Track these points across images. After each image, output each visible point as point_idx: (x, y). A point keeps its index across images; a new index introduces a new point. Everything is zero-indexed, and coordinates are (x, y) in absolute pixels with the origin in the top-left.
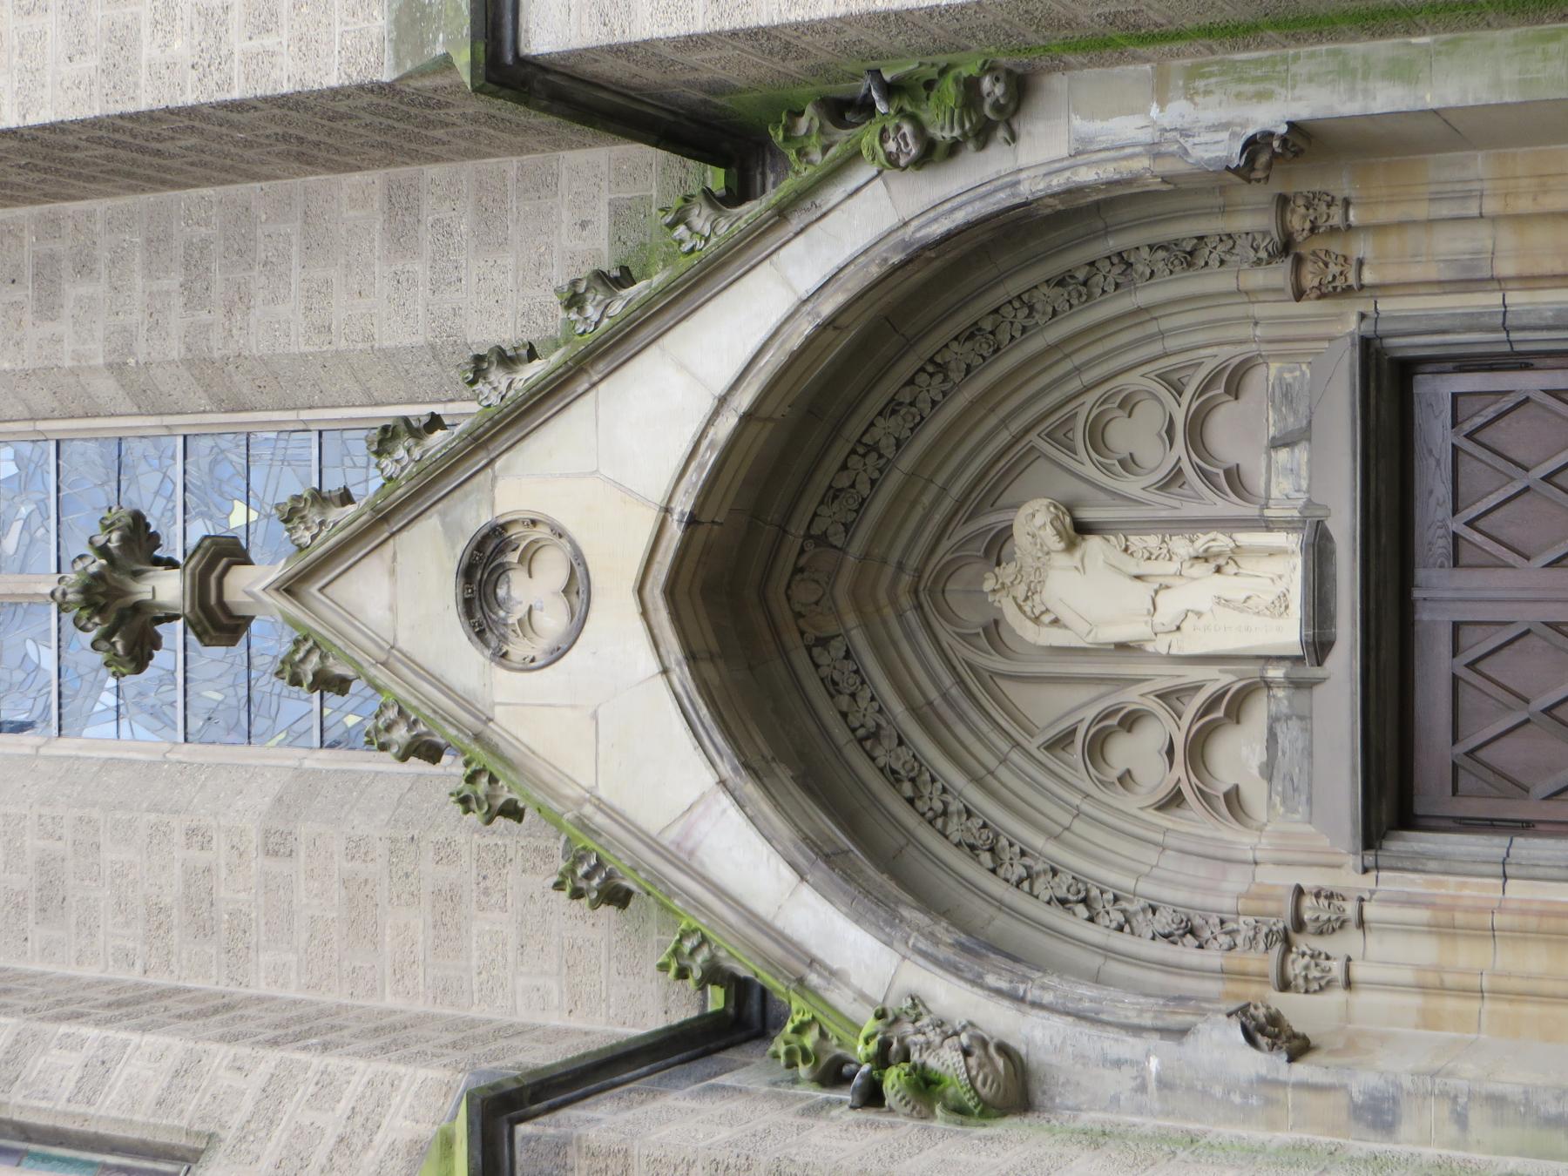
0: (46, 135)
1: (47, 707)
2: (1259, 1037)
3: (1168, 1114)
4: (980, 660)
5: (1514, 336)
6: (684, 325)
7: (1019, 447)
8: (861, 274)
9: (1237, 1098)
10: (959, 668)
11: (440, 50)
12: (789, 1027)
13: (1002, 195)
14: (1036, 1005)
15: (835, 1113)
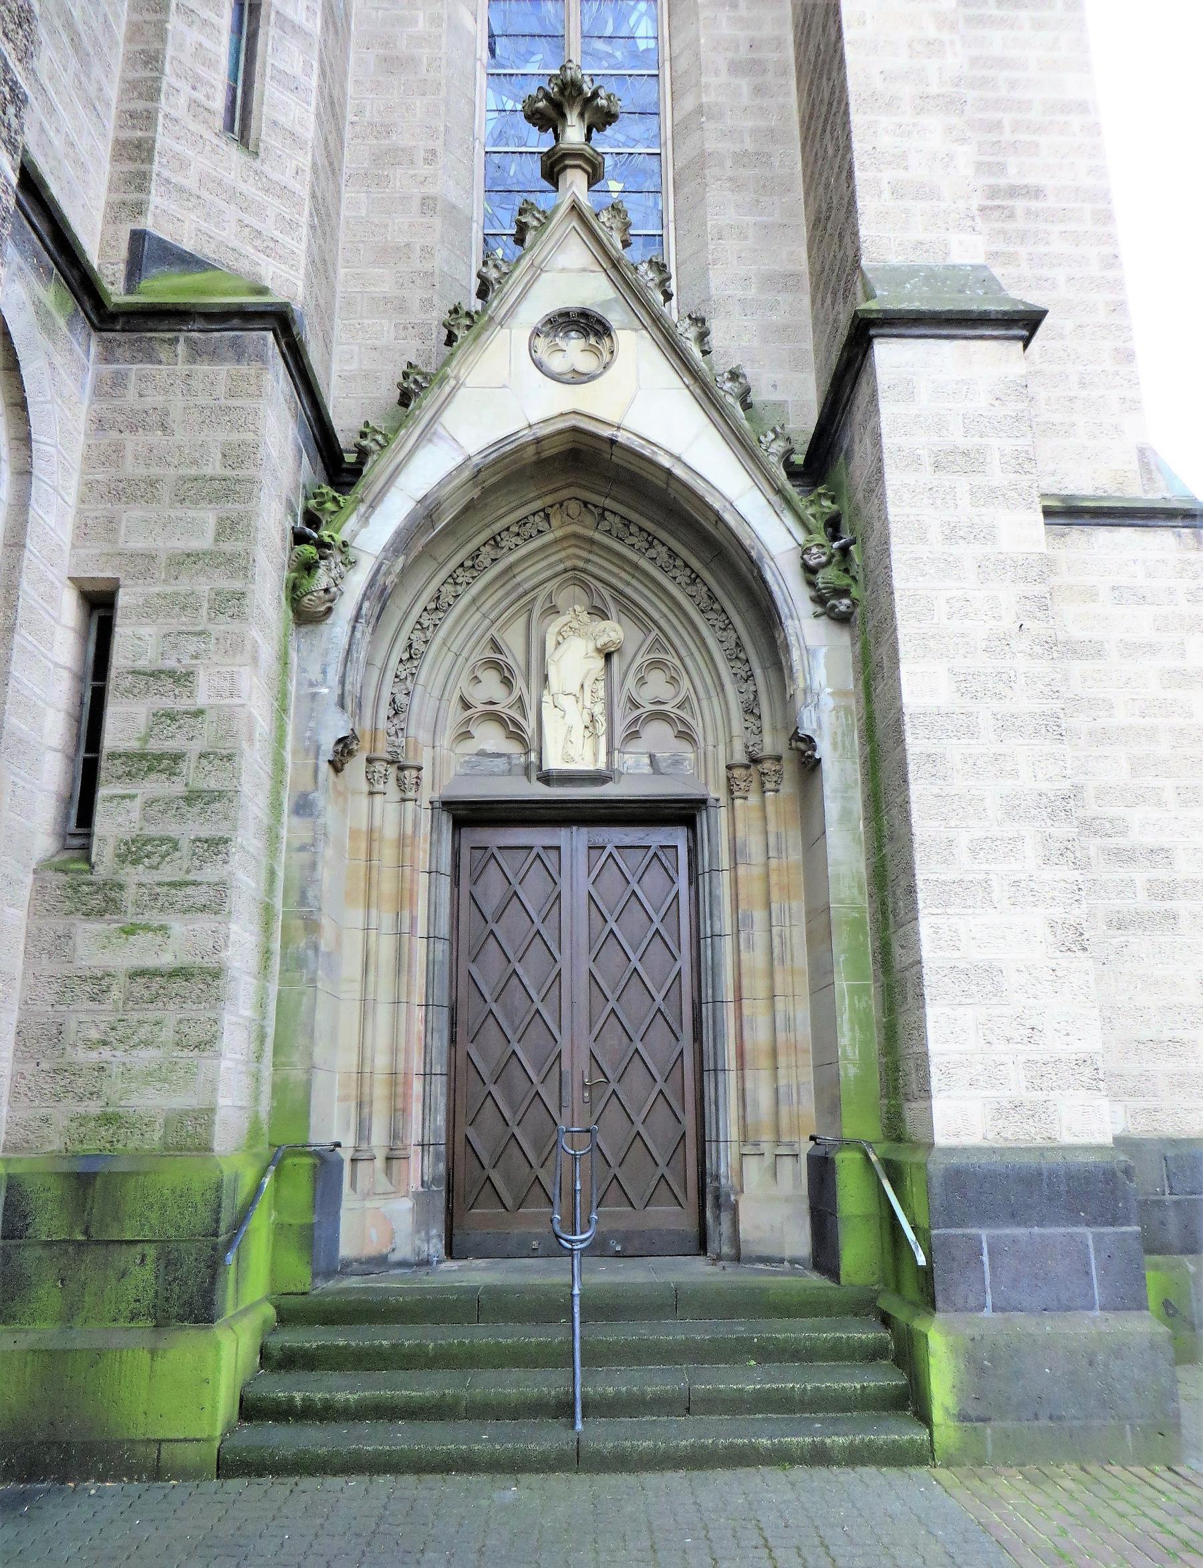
0: (838, 58)
1: (503, 67)
2: (342, 745)
3: (298, 698)
4: (539, 603)
5: (707, 875)
6: (720, 437)
7: (650, 623)
8: (746, 536)
9: (308, 734)
10: (533, 593)
11: (878, 292)
12: (336, 495)
13: (786, 610)
14: (354, 628)
15: (289, 518)
